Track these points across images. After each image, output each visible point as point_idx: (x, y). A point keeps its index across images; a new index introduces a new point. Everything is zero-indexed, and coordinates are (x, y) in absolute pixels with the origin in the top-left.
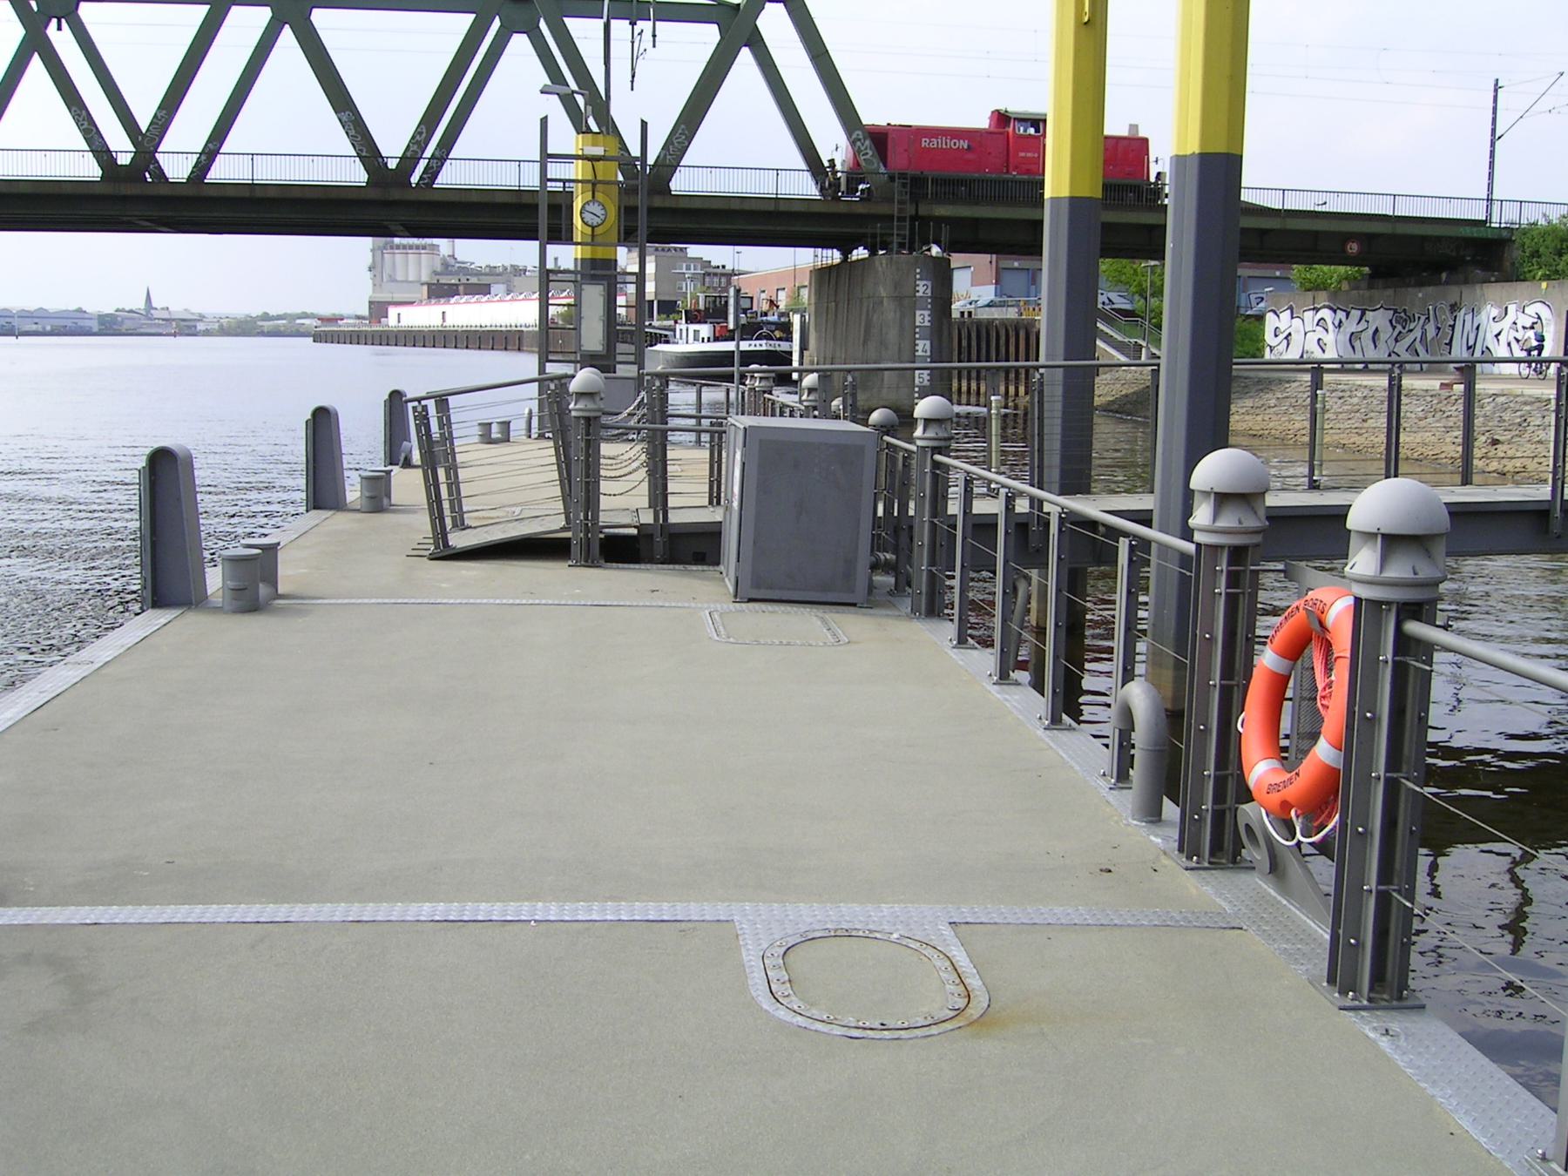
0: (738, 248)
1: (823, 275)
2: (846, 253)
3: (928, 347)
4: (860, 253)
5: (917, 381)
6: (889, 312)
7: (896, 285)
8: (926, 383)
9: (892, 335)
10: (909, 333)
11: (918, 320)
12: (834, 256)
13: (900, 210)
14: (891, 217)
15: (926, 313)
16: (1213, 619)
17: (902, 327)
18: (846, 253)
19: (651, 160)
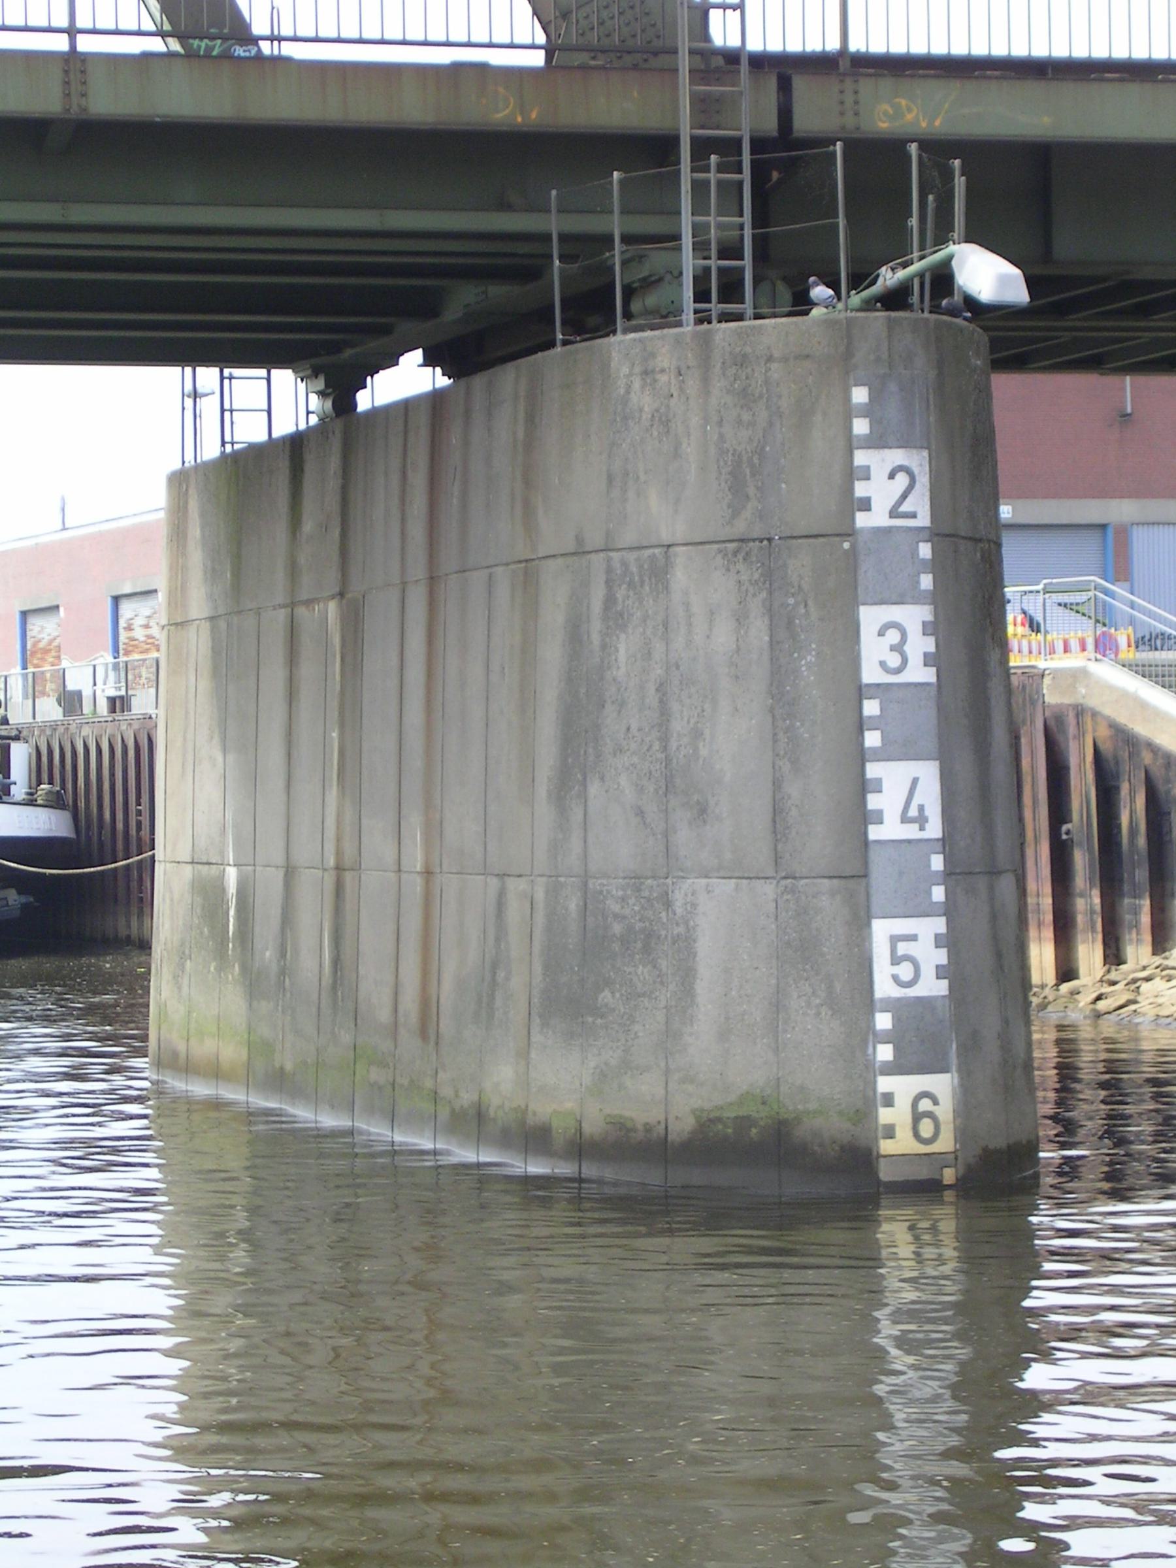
0: (1128, 388)
1: (241, 489)
2: (341, 387)
3: (930, 796)
4: (407, 378)
5: (884, 987)
6: (709, 617)
7: (743, 475)
8: (933, 987)
9: (731, 741)
10: (818, 723)
11: (875, 659)
12: (275, 402)
13: (703, 106)
14: (657, 149)
15: (913, 616)
16: (332, 754)
17: (782, 703)
18: (341, 387)
19: (161, 1232)
